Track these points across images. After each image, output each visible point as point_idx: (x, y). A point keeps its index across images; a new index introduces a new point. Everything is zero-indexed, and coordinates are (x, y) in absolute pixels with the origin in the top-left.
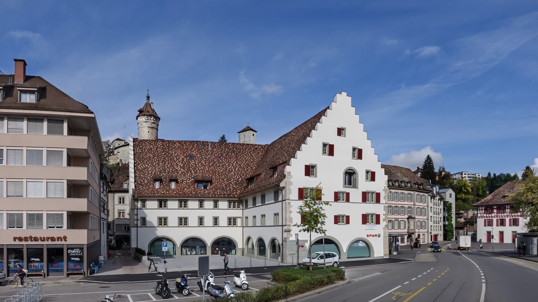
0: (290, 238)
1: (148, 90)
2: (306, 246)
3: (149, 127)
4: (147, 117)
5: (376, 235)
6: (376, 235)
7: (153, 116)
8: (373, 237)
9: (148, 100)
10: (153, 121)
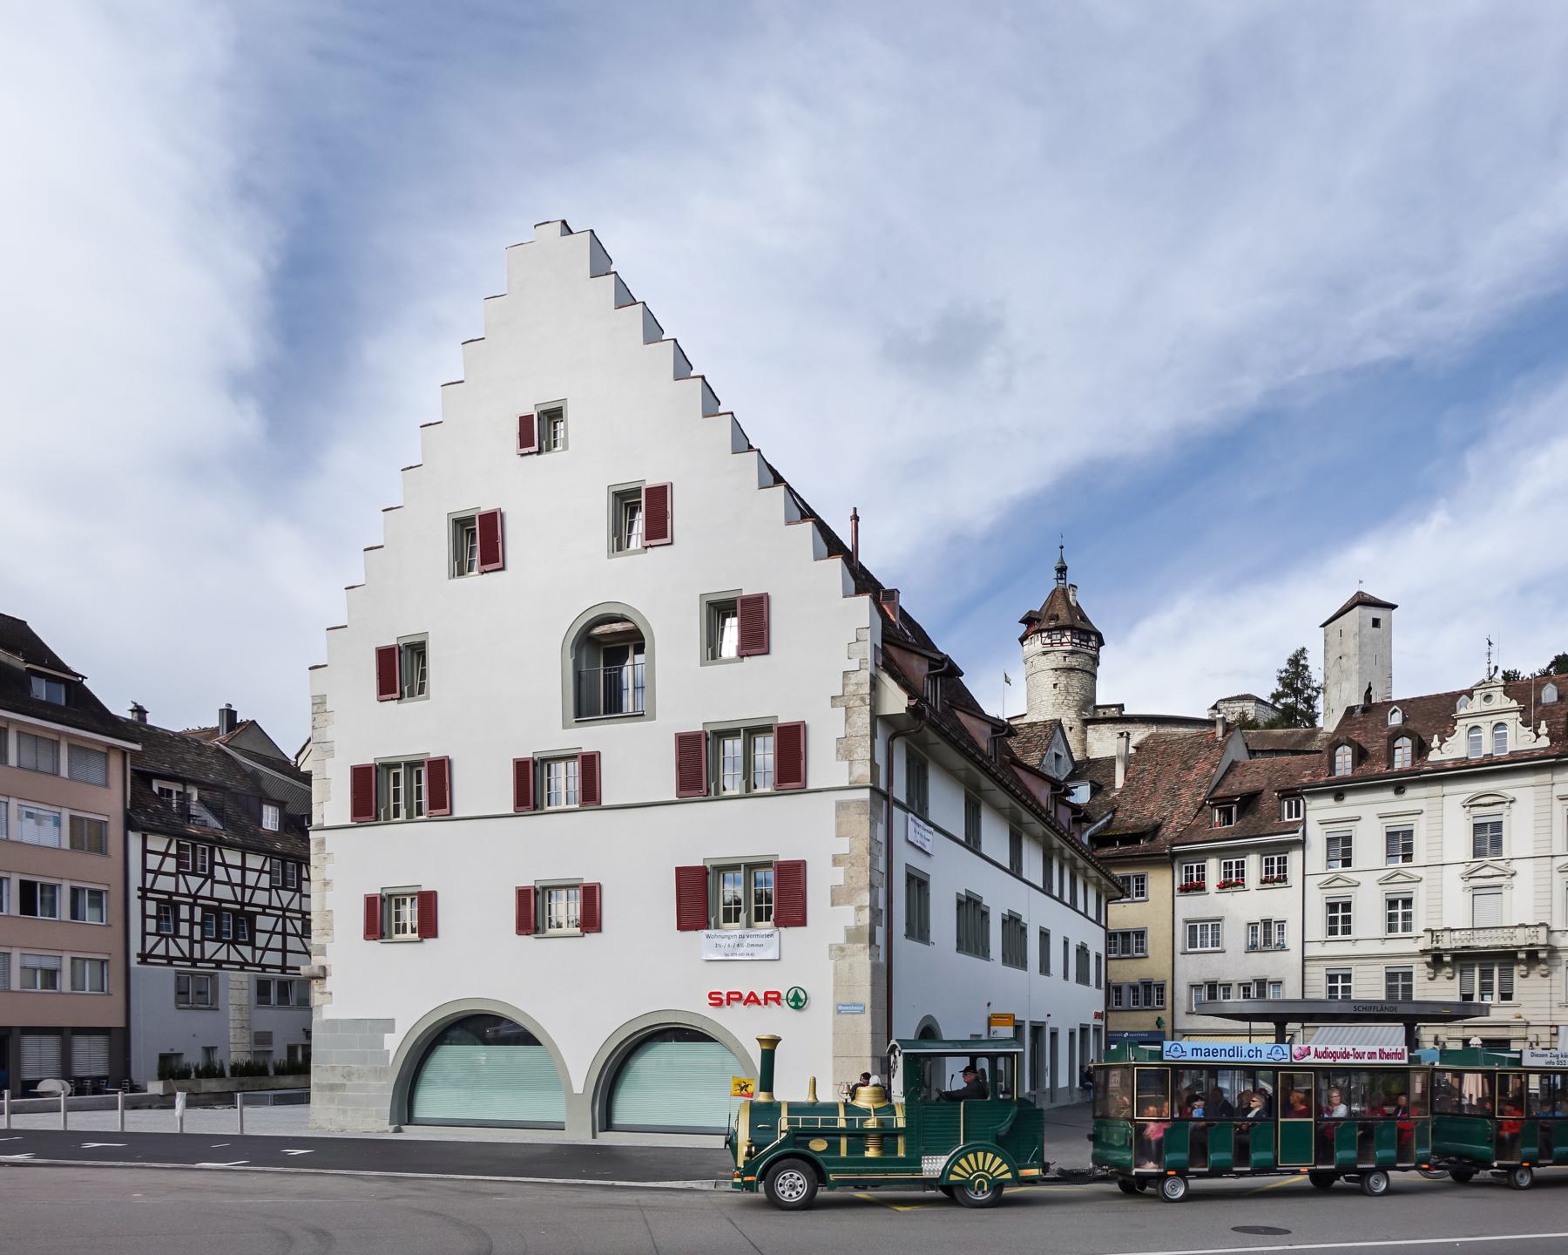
0: (326, 1007)
1: (1062, 547)
2: (388, 1051)
3: (1056, 670)
4: (1049, 637)
5: (773, 998)
6: (773, 998)
7: (1071, 628)
8: (755, 1007)
9: (1061, 579)
10: (1070, 648)
